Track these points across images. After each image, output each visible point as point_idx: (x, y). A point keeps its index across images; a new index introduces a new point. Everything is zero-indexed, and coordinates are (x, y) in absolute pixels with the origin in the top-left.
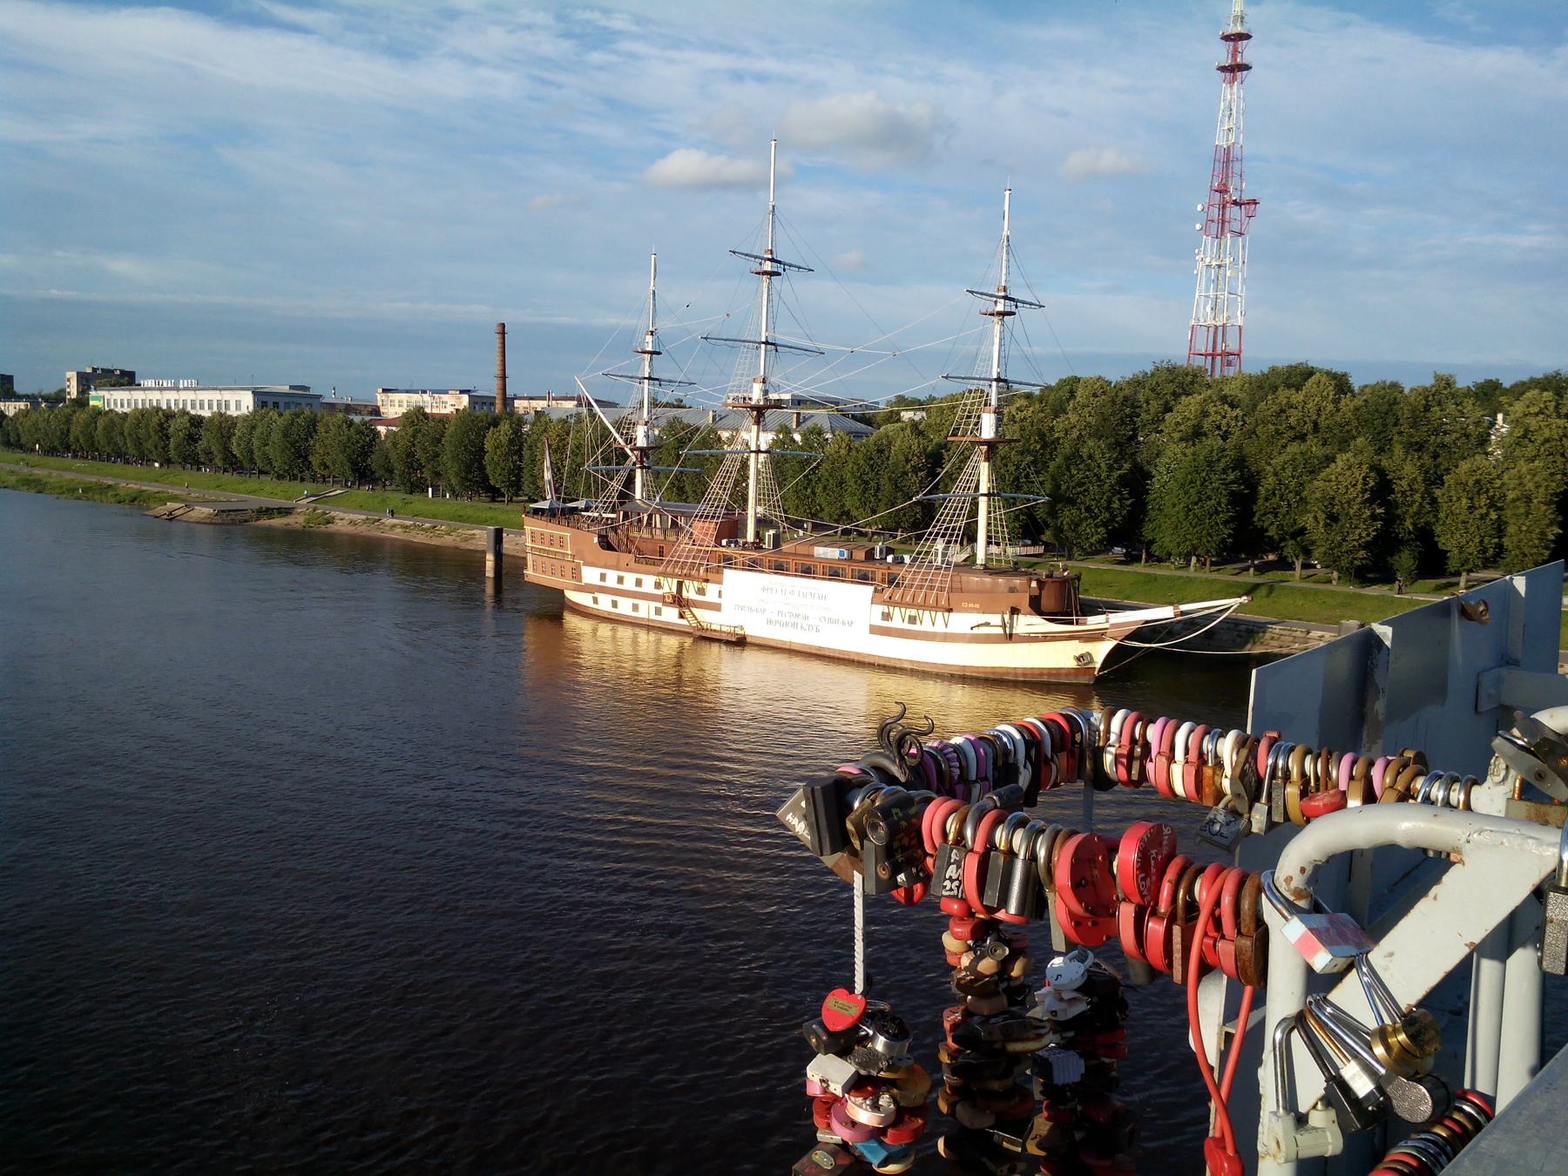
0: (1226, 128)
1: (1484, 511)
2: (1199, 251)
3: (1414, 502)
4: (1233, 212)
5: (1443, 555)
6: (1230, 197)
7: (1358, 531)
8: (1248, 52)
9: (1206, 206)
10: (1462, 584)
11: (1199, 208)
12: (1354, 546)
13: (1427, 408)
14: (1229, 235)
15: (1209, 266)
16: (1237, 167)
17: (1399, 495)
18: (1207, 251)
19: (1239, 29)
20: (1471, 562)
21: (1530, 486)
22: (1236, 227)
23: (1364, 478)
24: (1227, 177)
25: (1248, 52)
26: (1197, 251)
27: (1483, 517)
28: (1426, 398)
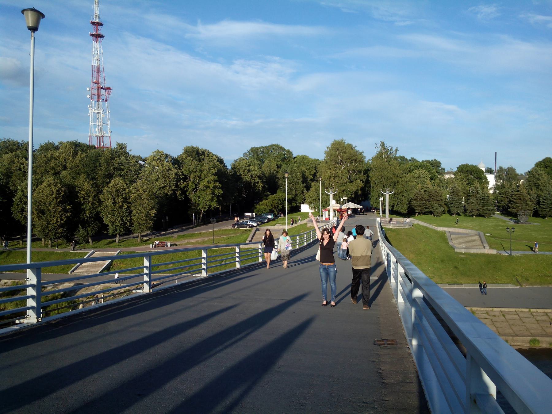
0: (96, 59)
1: (120, 204)
2: (90, 106)
3: (89, 202)
4: (103, 92)
5: (106, 227)
6: (100, 86)
7: (55, 219)
8: (102, 31)
9: (91, 88)
10: (117, 241)
11: (88, 89)
12: (55, 226)
13: (113, 158)
14: (101, 100)
15: (94, 112)
16: (102, 75)
17: (82, 199)
18: (92, 107)
19: (97, 21)
20: (118, 230)
21: (141, 191)
22: (104, 97)
23: (58, 191)
24: (99, 79)
25: (102, 31)
26: (89, 106)
27: (121, 207)
28: (112, 155)
